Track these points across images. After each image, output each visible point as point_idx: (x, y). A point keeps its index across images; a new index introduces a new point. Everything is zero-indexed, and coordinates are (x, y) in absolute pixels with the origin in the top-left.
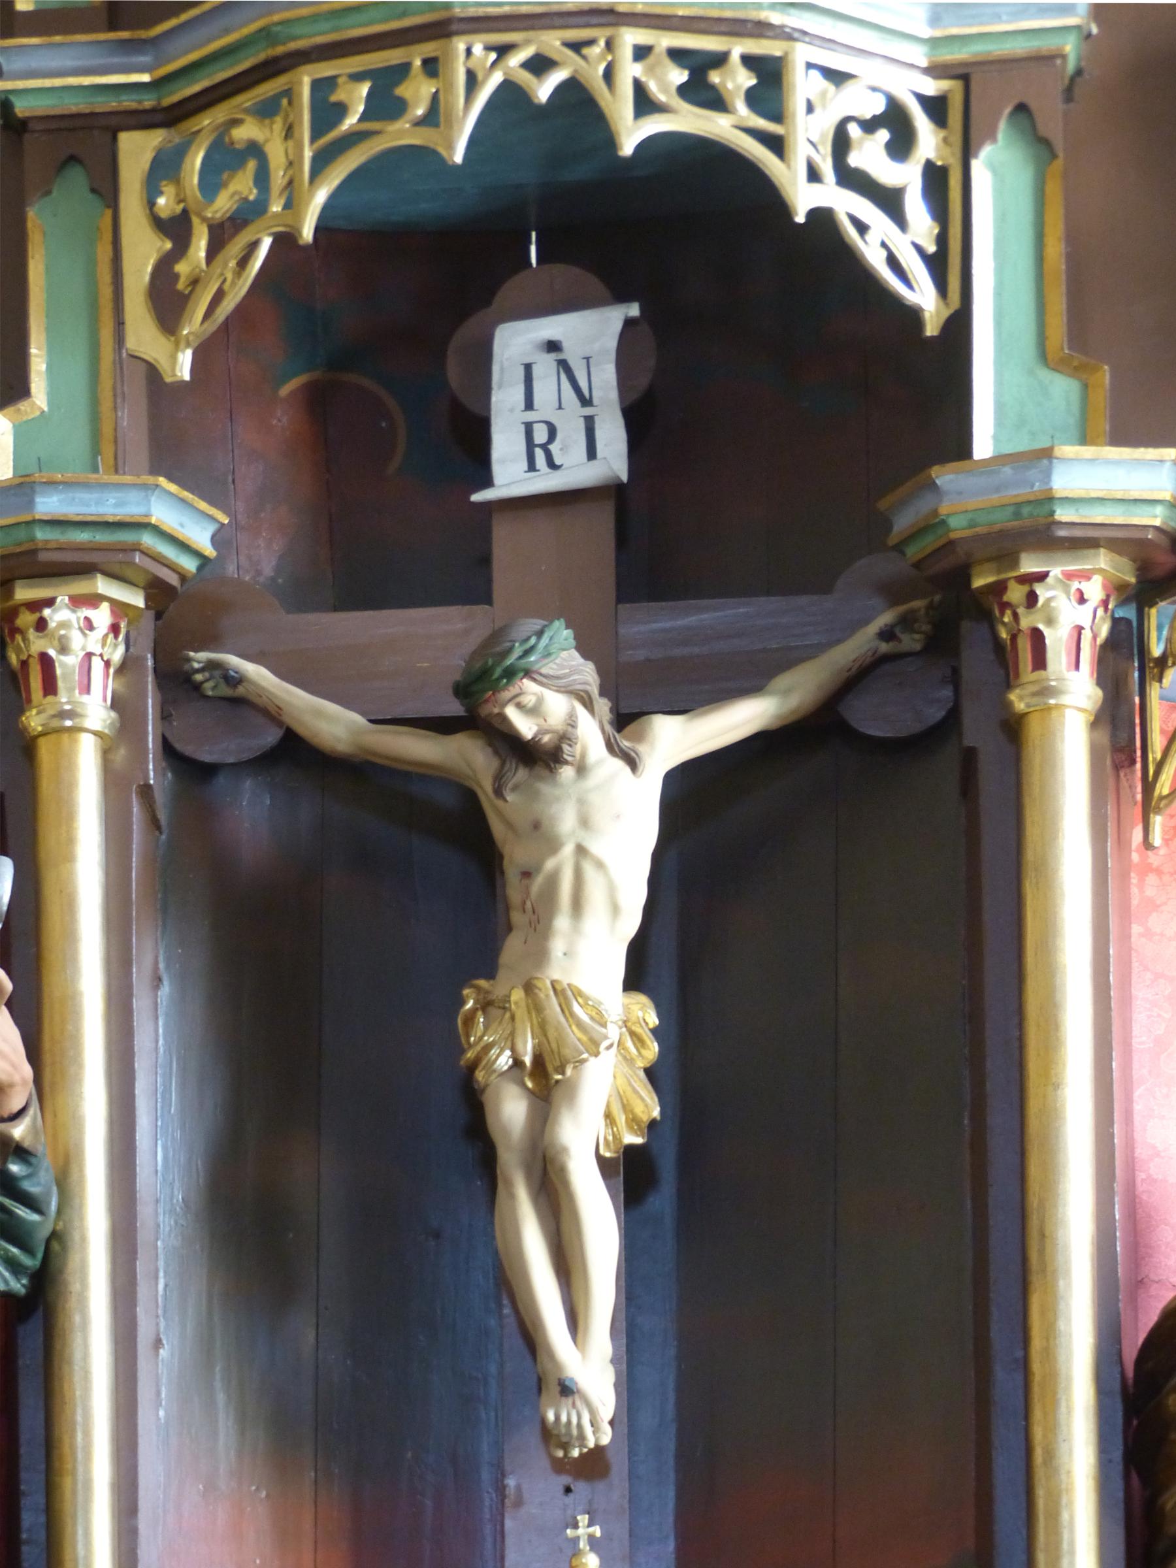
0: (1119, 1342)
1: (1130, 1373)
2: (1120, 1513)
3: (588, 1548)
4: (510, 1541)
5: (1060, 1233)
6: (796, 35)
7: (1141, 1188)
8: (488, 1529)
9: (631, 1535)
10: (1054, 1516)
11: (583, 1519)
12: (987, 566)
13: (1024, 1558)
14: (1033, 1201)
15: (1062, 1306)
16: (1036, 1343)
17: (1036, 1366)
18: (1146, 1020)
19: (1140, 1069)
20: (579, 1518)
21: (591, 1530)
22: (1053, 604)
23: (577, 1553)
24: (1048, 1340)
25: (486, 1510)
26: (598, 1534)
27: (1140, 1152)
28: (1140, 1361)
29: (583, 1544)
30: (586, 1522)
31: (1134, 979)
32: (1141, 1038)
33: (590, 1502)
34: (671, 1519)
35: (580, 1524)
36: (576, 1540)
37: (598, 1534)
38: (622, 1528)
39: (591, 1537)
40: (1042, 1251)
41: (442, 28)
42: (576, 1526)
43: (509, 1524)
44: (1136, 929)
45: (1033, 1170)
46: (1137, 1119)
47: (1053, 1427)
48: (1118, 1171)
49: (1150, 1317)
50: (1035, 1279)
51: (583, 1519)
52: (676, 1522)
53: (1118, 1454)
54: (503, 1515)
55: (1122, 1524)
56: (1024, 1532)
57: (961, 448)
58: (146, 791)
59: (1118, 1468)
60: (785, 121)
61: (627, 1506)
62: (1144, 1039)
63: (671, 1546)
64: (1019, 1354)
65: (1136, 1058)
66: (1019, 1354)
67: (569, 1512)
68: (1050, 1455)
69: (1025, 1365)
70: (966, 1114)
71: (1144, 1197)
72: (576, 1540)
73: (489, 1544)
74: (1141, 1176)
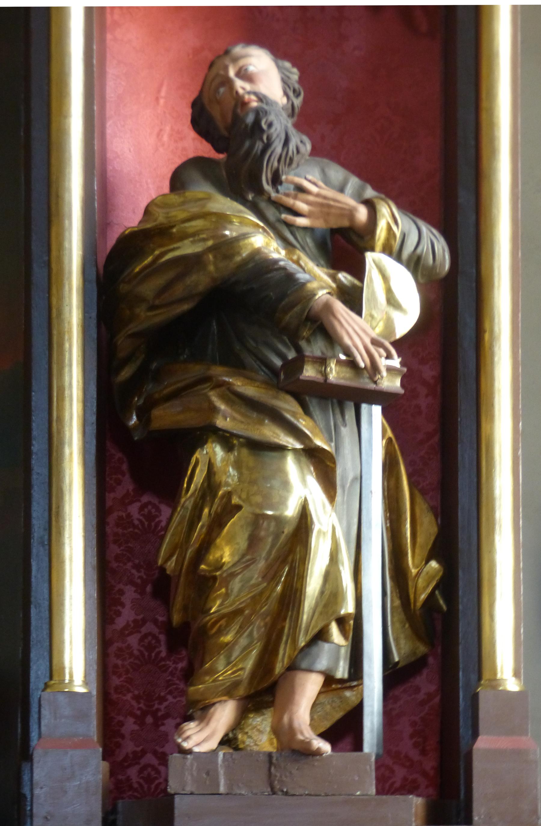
0: (96, 254)
1: (101, 271)
2: (94, 346)
5: (67, 195)
6: (264, 101)
7: (109, 174)
10: (61, 345)
13: (47, 366)
14: (54, 177)
15: (67, 234)
16: (54, 253)
17: (54, 266)
18: (113, 87)
19: (110, 110)
24: (59, 252)
27: (109, 155)
28: (105, 266)
31: (108, 63)
32: (111, 93)
40: (57, 204)
41: (451, 197)
44: (109, 36)
45: (53, 161)
46: (108, 137)
47: (61, 298)
48: (96, 164)
49: (111, 242)
50: (53, 219)
53: (94, 314)
55: (96, 351)
56: (47, 353)
59: (94, 322)
62: (113, 95)
64: (46, 258)
65: (108, 105)
66: (46, 258)
68: (60, 313)
69: (48, 264)
70: (22, 130)
71: (111, 179)
74: (109, 168)
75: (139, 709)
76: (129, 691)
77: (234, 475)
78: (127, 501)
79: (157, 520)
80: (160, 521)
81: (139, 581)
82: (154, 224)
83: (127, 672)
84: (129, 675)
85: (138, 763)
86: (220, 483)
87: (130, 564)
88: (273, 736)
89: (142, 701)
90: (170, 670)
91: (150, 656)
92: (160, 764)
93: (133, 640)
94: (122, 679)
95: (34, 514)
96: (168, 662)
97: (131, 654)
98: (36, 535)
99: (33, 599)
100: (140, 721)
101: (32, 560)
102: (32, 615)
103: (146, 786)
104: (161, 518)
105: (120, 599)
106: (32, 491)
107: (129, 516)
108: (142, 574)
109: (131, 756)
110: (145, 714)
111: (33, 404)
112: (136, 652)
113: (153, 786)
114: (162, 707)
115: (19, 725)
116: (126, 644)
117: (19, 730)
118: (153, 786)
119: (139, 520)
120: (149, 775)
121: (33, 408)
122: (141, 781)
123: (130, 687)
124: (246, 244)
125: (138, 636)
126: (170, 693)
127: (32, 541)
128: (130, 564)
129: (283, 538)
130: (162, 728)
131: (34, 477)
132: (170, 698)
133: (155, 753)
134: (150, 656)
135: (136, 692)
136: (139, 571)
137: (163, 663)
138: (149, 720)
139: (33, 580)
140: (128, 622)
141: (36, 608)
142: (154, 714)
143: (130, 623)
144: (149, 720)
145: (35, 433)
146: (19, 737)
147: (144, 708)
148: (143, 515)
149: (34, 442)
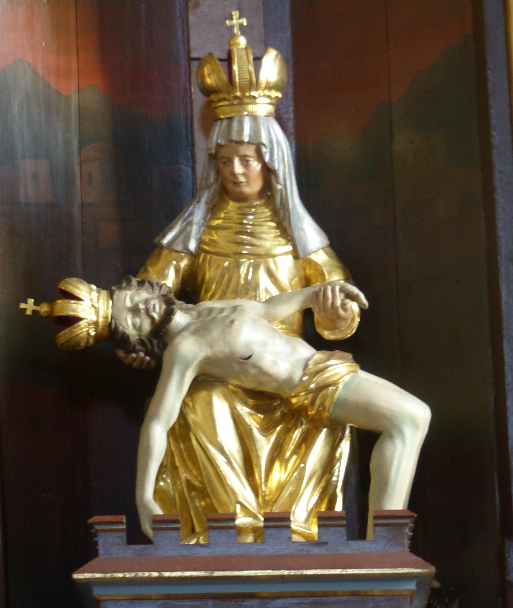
3: (239, 33)
4: (193, 30)
8: (179, 23)
9: (265, 26)
11: (236, 14)
12: (226, 172)
20: (233, 13)
21: (241, 21)
22: (241, 184)
23: (233, 36)
25: (178, 10)
26: (245, 23)
29: (236, 30)
30: (238, 16)
33: (239, 4)
34: (288, 16)
35: (234, 17)
36: (232, 27)
37: (245, 23)
38: (259, 20)
39: (241, 26)
42: (231, 19)
43: (191, 18)
51: (236, 14)
52: (292, 16)
54: (187, 14)
57: (123, 497)
58: (35, 72)
60: (140, 287)
61: (261, 6)
63: (289, 33)
67: (227, 11)
72: (232, 27)
73: (180, 32)
77: (225, 213)
82: (206, 74)
86: (139, 339)
88: (134, 281)
95: (500, 224)
98: (503, 249)
99: (505, 332)
101: (500, 283)
102: (505, 352)
106: (495, 195)
111: (490, 85)
115: (497, 494)
117: (497, 501)
121: (490, 90)
124: (338, 398)
127: (499, 257)
131: (497, 176)
139: (504, 307)
141: (509, 343)
145: (494, 121)
146: (498, 508)
149: (494, 133)
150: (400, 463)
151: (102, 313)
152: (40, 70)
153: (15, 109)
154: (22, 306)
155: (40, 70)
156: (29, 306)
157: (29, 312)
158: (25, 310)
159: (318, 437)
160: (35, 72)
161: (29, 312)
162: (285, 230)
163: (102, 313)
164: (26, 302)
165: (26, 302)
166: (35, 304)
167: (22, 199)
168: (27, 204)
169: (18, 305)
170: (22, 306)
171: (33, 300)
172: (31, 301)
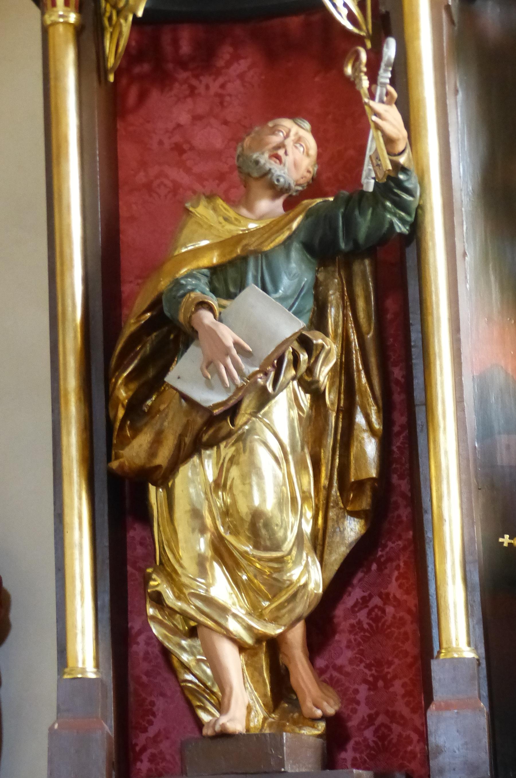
58: (507, 374)
75: (372, 675)
76: (361, 661)
78: (363, 727)
79: (383, 620)
80: (386, 621)
81: (371, 679)
83: (359, 644)
84: (361, 647)
85: (367, 606)
87: (362, 665)
89: (374, 668)
90: (395, 635)
91: (377, 627)
92: (385, 604)
93: (368, 733)
94: (355, 652)
96: (393, 629)
97: (362, 629)
100: (373, 686)
103: (374, 625)
104: (392, 736)
105: (355, 698)
107: (360, 622)
108: (374, 672)
109: (360, 600)
110: (376, 679)
112: (366, 626)
113: (380, 625)
114: (390, 670)
116: (357, 620)
118: (380, 625)
119: (374, 741)
120: (377, 615)
122: (371, 622)
123: (362, 657)
125: (372, 728)
126: (397, 656)
128: (362, 665)
129: (454, 10)
130: (391, 690)
132: (396, 661)
133: (380, 595)
134: (377, 627)
135: (368, 662)
136: (370, 670)
137: (389, 630)
138: (380, 684)
140: (357, 599)
142: (384, 678)
143: (366, 718)
144: (380, 684)
146: (136, 362)
147: (376, 674)
148: (372, 619)
150: (440, 507)
151: (348, 522)
152: (510, 371)
153: (493, 399)
154: (501, 540)
155: (510, 371)
156: (506, 540)
157: (506, 545)
158: (503, 543)
159: (289, 430)
160: (507, 374)
161: (506, 545)
162: (243, 614)
163: (348, 522)
164: (503, 537)
165: (503, 537)
166: (510, 538)
167: (499, 463)
168: (502, 467)
169: (498, 539)
170: (501, 540)
171: (508, 536)
172: (507, 536)
